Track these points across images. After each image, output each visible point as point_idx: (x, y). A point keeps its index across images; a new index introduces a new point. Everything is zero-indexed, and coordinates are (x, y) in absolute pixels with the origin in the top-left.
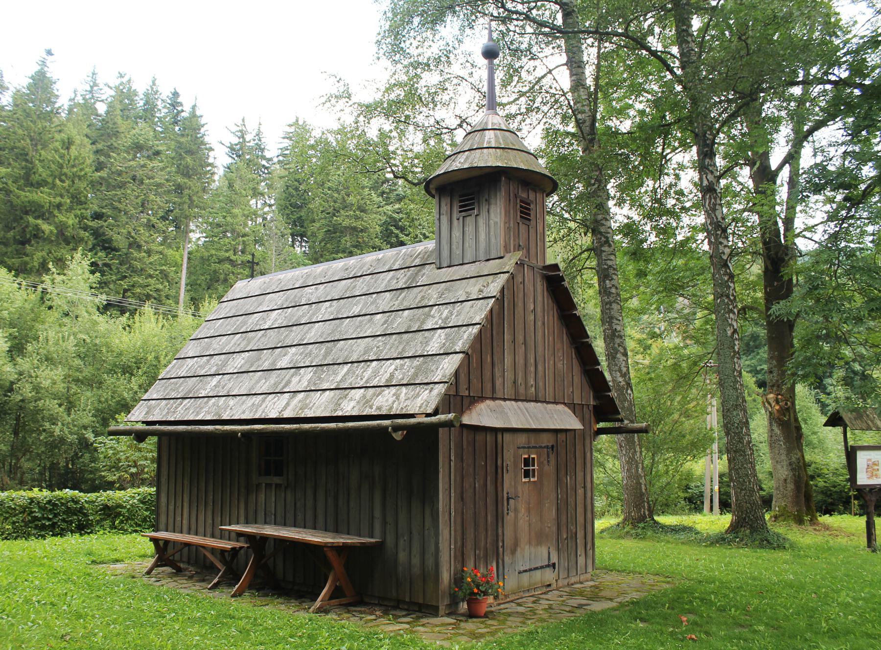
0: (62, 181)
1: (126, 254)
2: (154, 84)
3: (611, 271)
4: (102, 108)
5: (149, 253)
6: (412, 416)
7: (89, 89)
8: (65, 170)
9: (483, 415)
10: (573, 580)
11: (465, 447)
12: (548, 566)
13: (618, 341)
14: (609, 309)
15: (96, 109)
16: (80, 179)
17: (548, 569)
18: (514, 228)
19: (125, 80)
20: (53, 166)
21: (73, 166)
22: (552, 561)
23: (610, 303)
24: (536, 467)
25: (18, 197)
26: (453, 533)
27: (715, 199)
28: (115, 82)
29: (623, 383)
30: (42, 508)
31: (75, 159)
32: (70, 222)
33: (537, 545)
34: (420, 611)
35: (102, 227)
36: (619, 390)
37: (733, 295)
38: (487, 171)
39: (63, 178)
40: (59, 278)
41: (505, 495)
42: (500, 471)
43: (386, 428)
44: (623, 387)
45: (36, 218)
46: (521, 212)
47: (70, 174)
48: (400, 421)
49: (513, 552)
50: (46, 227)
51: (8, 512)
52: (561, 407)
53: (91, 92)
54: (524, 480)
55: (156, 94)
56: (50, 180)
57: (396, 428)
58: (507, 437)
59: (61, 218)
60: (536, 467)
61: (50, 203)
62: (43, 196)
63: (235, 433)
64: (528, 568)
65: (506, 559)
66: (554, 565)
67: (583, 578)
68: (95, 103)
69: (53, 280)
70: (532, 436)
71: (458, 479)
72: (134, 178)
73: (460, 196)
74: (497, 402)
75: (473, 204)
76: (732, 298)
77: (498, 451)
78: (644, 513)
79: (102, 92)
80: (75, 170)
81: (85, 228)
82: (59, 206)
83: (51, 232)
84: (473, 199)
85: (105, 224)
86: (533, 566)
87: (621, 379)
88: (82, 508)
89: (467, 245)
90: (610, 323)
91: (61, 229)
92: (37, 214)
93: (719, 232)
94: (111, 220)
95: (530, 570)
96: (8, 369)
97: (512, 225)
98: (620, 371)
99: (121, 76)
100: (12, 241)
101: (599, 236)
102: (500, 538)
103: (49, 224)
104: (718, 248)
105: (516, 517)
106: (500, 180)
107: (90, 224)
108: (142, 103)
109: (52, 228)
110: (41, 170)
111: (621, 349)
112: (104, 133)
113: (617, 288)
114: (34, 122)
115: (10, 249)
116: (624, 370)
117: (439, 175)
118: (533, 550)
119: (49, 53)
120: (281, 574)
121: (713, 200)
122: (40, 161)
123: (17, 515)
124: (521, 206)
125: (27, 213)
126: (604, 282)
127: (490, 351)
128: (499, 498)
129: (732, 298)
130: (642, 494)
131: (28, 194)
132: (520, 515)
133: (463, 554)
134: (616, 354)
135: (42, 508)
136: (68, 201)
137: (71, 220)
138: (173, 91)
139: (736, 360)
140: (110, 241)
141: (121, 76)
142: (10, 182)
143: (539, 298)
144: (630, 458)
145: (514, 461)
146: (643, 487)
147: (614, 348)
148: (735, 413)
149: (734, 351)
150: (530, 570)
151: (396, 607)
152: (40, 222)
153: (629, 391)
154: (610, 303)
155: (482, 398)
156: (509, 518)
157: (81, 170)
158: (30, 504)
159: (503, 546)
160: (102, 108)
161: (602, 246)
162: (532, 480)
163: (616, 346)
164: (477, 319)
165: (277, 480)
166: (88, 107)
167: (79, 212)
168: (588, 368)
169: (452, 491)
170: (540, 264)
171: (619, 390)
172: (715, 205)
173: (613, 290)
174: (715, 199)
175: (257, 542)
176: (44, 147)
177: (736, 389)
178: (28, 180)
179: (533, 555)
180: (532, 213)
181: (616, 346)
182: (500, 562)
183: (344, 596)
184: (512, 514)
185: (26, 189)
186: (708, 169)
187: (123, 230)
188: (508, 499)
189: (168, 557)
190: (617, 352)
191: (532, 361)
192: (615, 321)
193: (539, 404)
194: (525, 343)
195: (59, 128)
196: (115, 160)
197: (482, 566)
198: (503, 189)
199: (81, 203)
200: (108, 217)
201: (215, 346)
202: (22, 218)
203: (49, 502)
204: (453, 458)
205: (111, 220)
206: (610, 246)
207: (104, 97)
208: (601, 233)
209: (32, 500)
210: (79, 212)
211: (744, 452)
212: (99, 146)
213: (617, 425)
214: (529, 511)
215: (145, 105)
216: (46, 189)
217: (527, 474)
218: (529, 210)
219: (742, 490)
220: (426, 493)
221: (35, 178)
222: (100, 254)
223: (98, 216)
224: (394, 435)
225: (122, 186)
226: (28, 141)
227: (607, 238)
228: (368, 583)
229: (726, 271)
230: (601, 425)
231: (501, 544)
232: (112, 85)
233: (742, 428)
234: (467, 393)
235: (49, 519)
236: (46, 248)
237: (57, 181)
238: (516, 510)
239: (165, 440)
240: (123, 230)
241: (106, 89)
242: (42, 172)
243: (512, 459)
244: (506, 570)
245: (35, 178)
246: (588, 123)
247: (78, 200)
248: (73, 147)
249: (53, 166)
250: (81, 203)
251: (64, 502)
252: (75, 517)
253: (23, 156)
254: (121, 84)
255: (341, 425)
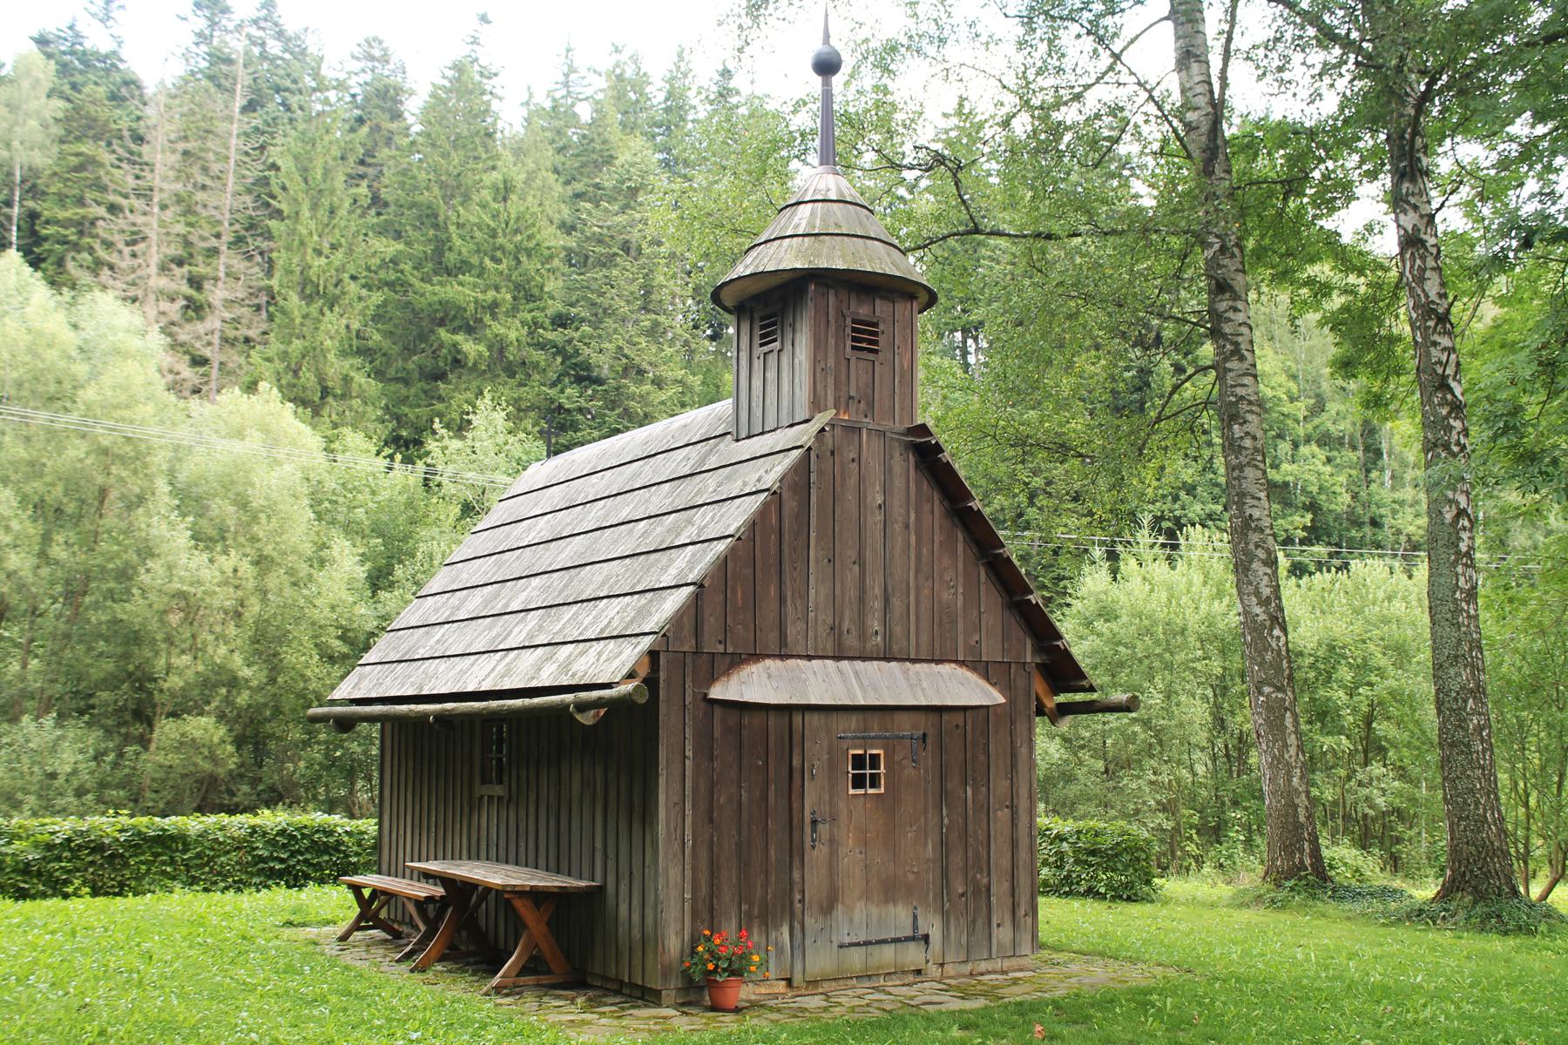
0: (498, 261)
1: (617, 389)
2: (680, 57)
3: (1244, 406)
4: (585, 112)
5: (658, 383)
6: (608, 686)
7: (562, 79)
8: (500, 240)
9: (756, 684)
10: (983, 966)
11: (717, 734)
12: (913, 939)
13: (1254, 537)
14: (1238, 478)
15: (575, 115)
16: (529, 256)
17: (912, 945)
18: (837, 369)
19: (624, 57)
20: (478, 234)
21: (517, 231)
22: (921, 932)
23: (1241, 467)
24: (882, 770)
25: (423, 295)
26: (688, 873)
27: (1423, 258)
28: (606, 63)
29: (1263, 617)
30: (272, 843)
31: (518, 219)
32: (513, 335)
33: (886, 901)
34: (642, 998)
35: (570, 341)
36: (1255, 630)
37: (1458, 443)
38: (786, 276)
39: (499, 254)
40: (456, 444)
41: (808, 818)
42: (796, 776)
43: (564, 707)
44: (1262, 625)
45: (455, 331)
46: (854, 339)
47: (510, 247)
48: (583, 695)
49: (828, 908)
50: (471, 348)
51: (212, 849)
52: (946, 669)
53: (566, 85)
54: (852, 792)
55: (685, 76)
56: (475, 260)
57: (582, 707)
58: (814, 720)
59: (498, 328)
60: (882, 770)
61: (476, 302)
62: (462, 291)
63: (426, 715)
64: (862, 939)
65: (809, 921)
66: (926, 938)
67: (1007, 964)
68: (573, 105)
69: (444, 449)
70: (875, 720)
71: (702, 787)
72: (626, 247)
73: (762, 319)
74: (791, 662)
75: (774, 332)
76: (1456, 449)
77: (792, 742)
78: (1301, 861)
79: (585, 82)
80: (519, 237)
81: (541, 346)
82: (493, 307)
83: (480, 355)
84: (774, 324)
85: (577, 335)
86: (873, 938)
87: (1258, 610)
88: (339, 843)
89: (768, 401)
90: (1241, 505)
91: (499, 347)
92: (457, 323)
93: (1431, 323)
94: (586, 328)
95: (867, 943)
96: (363, 611)
97: (831, 362)
98: (1257, 594)
99: (617, 50)
100: (416, 375)
101: (1221, 342)
102: (797, 888)
103: (477, 341)
104: (1428, 354)
105: (833, 854)
106: (806, 291)
107: (550, 336)
108: (661, 96)
109: (482, 348)
110: (458, 242)
111: (1261, 554)
112: (584, 161)
113: (1254, 438)
114: (446, 156)
115: (413, 391)
116: (1266, 592)
117: (732, 281)
118: (874, 910)
119: (484, 19)
120: (464, 934)
121: (1418, 262)
122: (459, 225)
123: (228, 852)
124: (854, 330)
125: (442, 323)
126: (1230, 427)
127: (775, 579)
128: (795, 821)
129: (1456, 449)
130: (1298, 826)
131: (437, 288)
132: (843, 850)
133: (711, 908)
134: (1251, 562)
135: (272, 843)
136: (508, 297)
137: (512, 331)
138: (721, 68)
139: (1460, 569)
140: (587, 366)
141: (617, 50)
142: (407, 267)
143: (898, 483)
144: (1274, 757)
145: (830, 759)
146: (1302, 812)
147: (1246, 552)
148: (1452, 672)
149: (1458, 553)
150: (867, 943)
151: (608, 992)
152: (459, 338)
153: (1277, 632)
154: (1241, 467)
155: (756, 657)
156: (817, 855)
157: (530, 238)
158: (251, 835)
159: (802, 901)
160: (585, 112)
161: (1226, 360)
162: (871, 791)
163: (1252, 547)
164: (731, 531)
165: (498, 790)
166: (559, 113)
167: (529, 317)
168: (1016, 598)
169: (688, 806)
170: (900, 426)
171: (1255, 630)
172: (1423, 270)
173: (1248, 443)
174: (1423, 258)
175: (459, 890)
176: (466, 198)
177: (1459, 626)
178: (441, 264)
179: (875, 919)
180: (882, 339)
181: (1252, 547)
182: (797, 925)
183: (549, 972)
184: (822, 850)
185: (435, 279)
186: (1408, 203)
187: (606, 345)
188: (814, 822)
189: (374, 912)
190: (1251, 557)
191: (878, 591)
192: (1249, 501)
193: (894, 664)
194: (861, 561)
195: (490, 163)
196: (590, 214)
197: (756, 930)
198: (811, 305)
199: (530, 298)
200: (583, 320)
201: (465, 576)
202: (433, 331)
203: (282, 832)
204: (689, 753)
205: (586, 328)
206: (1242, 359)
207: (589, 92)
208: (1224, 336)
209: (254, 830)
210: (529, 317)
211: (1468, 746)
212: (579, 187)
213: (1079, 697)
214: (864, 843)
215: (667, 100)
216: (467, 278)
217: (858, 782)
218: (875, 334)
219: (1461, 819)
220: (644, 811)
221: (451, 258)
222: (568, 391)
223: (561, 321)
224: (579, 717)
225: (607, 262)
226: (436, 190)
227: (1237, 344)
228: (573, 949)
229: (1444, 398)
230: (1062, 698)
231: (798, 897)
232: (602, 69)
233: (1465, 701)
234: (721, 649)
235: (282, 861)
236: (475, 384)
237: (487, 262)
238: (833, 841)
239: (388, 726)
240: (606, 345)
241: (592, 78)
242: (461, 246)
243: (826, 757)
244: (808, 942)
245: (451, 258)
246: (1204, 128)
247: (527, 293)
248: (514, 197)
249: (478, 234)
250: (530, 298)
251: (306, 832)
252: (326, 858)
253: (429, 217)
254: (617, 65)
255: (527, 701)
